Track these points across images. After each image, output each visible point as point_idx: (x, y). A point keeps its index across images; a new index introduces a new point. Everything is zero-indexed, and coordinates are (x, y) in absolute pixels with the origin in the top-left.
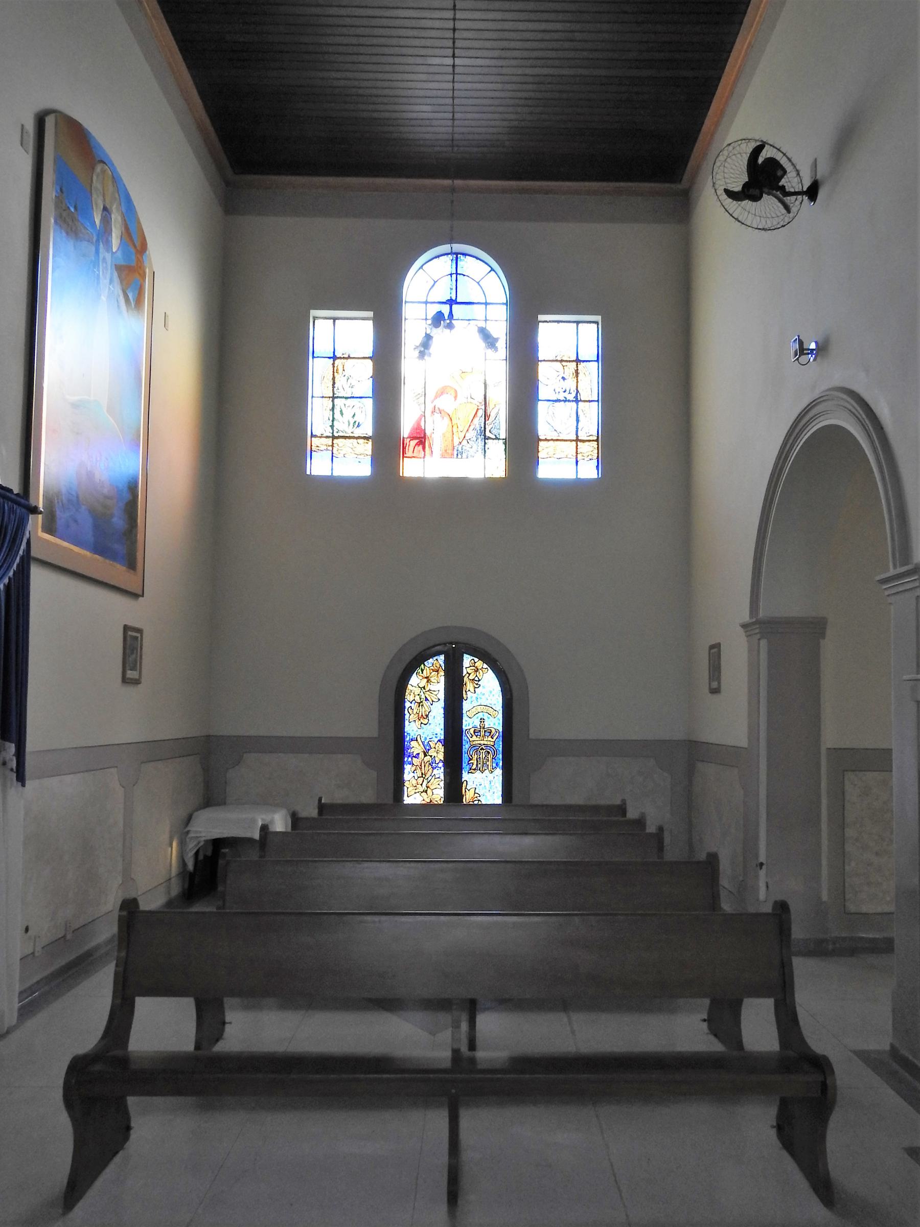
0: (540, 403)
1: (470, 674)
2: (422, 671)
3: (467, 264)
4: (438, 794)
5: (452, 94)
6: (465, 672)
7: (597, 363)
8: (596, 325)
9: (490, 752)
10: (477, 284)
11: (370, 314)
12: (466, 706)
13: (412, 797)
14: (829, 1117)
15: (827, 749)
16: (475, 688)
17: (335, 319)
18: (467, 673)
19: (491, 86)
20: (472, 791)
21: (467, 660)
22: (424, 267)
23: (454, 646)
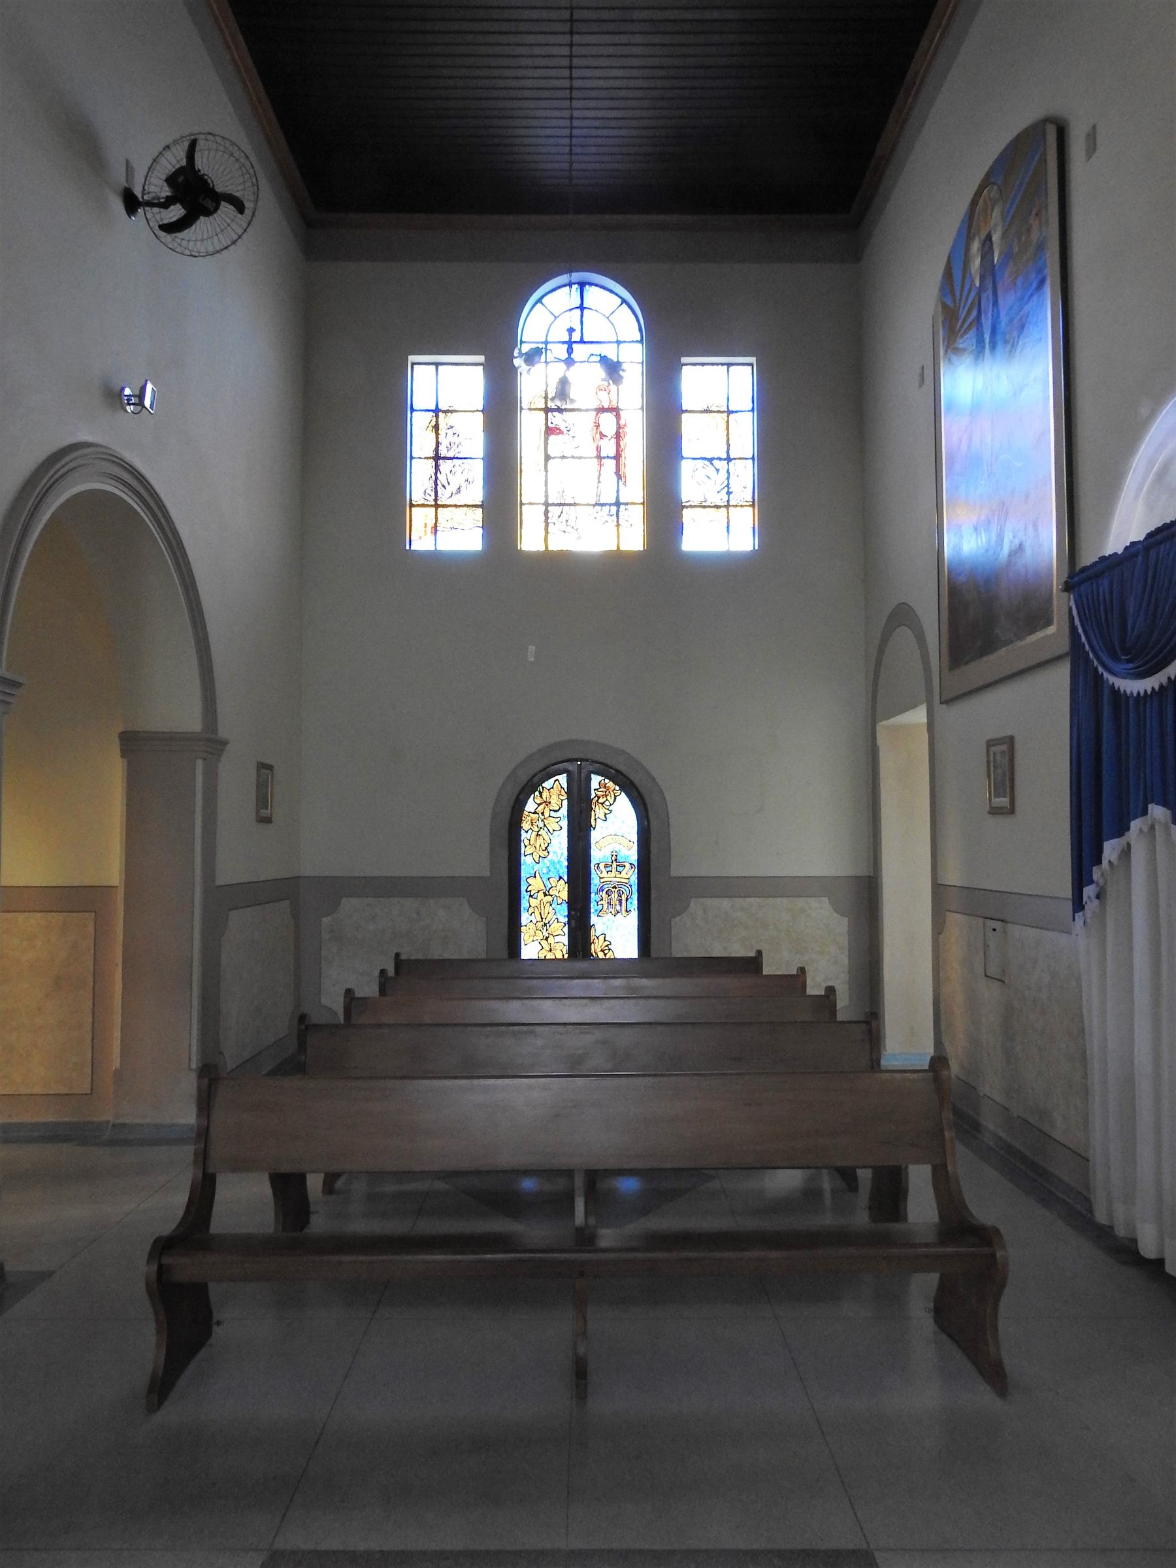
0: (482, 457)
1: (599, 798)
2: (541, 793)
3: (592, 293)
4: (560, 946)
5: (573, 72)
6: (593, 795)
7: (751, 413)
8: (750, 368)
9: (624, 891)
10: (606, 319)
11: (481, 359)
12: (595, 836)
13: (529, 951)
14: (880, 938)
15: (1070, 933)
16: (606, 814)
17: (437, 364)
18: (596, 796)
19: (630, 113)
20: (602, 938)
21: (596, 780)
22: (544, 300)
23: (579, 763)
